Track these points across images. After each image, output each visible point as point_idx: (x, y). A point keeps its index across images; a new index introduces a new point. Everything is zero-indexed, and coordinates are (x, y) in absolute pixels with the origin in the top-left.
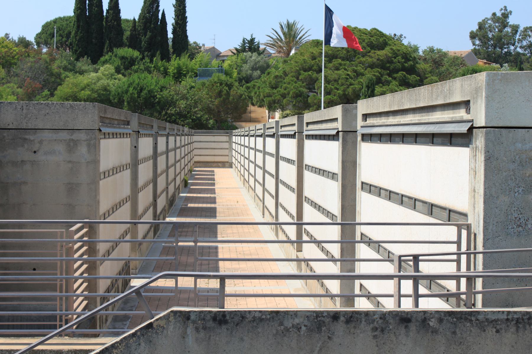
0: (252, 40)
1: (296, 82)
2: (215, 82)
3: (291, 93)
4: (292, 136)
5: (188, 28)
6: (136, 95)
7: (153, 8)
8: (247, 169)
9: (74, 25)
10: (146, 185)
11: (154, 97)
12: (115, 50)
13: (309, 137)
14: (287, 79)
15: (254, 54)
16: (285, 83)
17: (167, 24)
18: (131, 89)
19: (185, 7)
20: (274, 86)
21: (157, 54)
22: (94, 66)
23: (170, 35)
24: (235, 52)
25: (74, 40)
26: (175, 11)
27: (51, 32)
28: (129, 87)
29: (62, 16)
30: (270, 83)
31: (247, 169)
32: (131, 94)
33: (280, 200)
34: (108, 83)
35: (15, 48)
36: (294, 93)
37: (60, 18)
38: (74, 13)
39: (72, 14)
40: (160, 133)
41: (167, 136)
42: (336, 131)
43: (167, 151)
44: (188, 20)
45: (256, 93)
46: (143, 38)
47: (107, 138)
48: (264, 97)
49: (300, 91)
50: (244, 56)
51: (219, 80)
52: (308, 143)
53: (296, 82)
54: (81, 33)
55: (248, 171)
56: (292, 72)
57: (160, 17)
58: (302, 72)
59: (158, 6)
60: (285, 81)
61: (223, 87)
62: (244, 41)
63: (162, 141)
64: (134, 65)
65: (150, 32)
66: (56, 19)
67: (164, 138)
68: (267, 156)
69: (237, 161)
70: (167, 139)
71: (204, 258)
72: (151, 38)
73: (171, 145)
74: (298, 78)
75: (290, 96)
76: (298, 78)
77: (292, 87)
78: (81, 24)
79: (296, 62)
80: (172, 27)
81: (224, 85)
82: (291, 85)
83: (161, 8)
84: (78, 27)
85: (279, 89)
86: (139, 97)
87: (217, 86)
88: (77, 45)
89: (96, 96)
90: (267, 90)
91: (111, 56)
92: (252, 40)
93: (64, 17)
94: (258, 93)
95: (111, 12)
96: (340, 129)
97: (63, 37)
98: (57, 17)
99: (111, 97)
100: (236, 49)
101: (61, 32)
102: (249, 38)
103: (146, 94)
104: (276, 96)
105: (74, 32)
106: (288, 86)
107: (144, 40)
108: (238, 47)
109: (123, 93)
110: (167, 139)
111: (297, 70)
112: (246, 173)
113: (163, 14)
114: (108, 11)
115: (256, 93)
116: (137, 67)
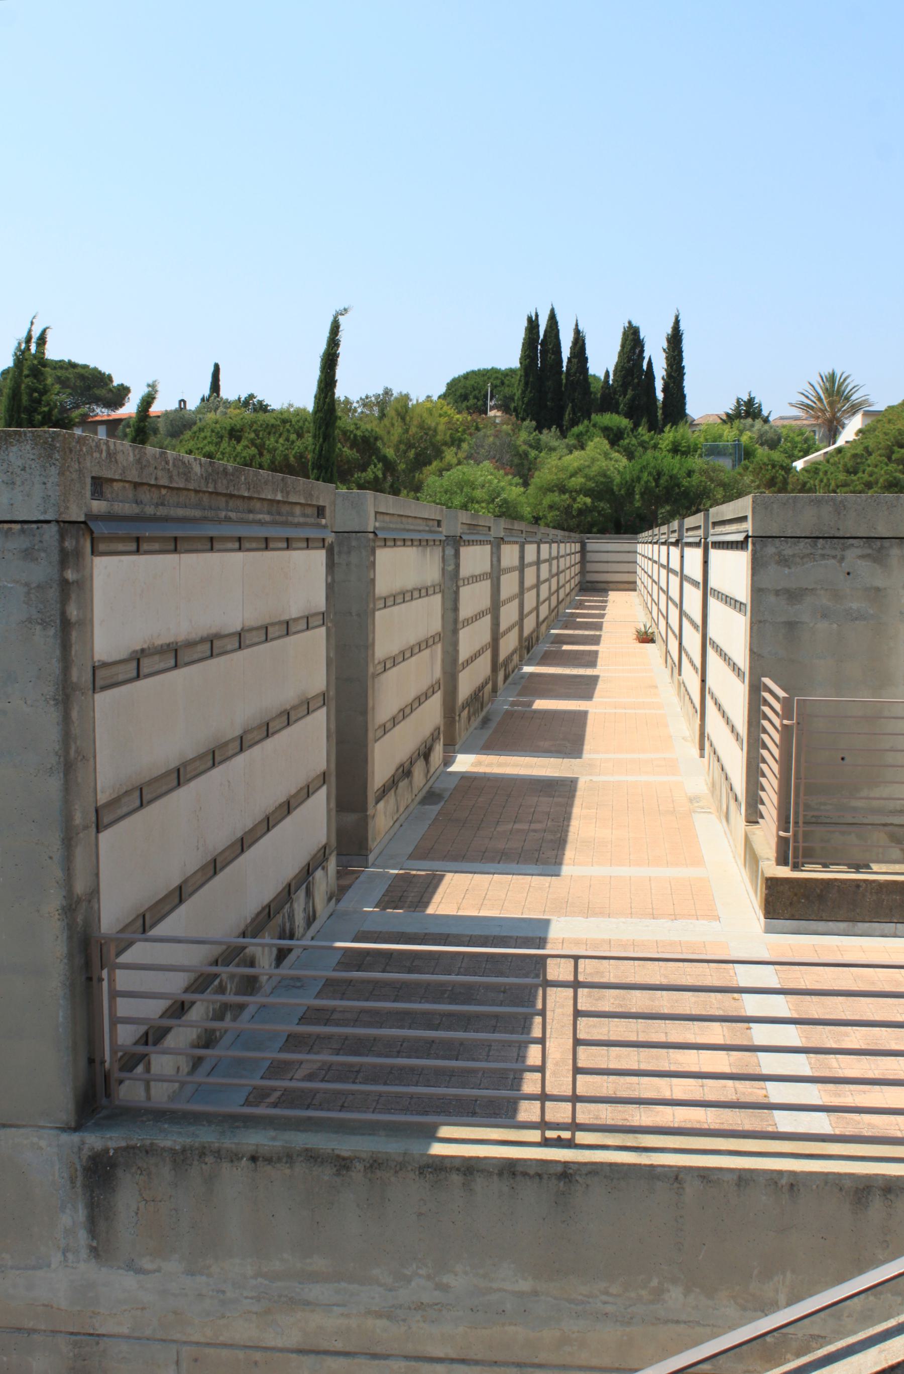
0: (750, 402)
1: (887, 465)
2: (764, 464)
3: (881, 480)
4: (697, 545)
5: (685, 383)
6: (654, 484)
7: (634, 353)
8: (665, 588)
9: (520, 381)
10: (530, 612)
11: (678, 485)
12: (593, 416)
13: (719, 545)
14: (872, 460)
15: (757, 421)
16: (869, 466)
17: (654, 378)
18: (645, 476)
19: (680, 352)
20: (851, 470)
21: (643, 423)
22: (567, 440)
23: (660, 395)
24: (724, 417)
25: (520, 403)
26: (667, 358)
27: (469, 392)
28: (641, 471)
29: (476, 369)
30: (845, 465)
31: (665, 588)
32: (646, 483)
33: (712, 633)
34: (607, 466)
35: (458, 416)
36: (886, 480)
37: (473, 372)
38: (521, 363)
39: (518, 365)
40: (528, 539)
41: (497, 544)
42: (744, 535)
43: (538, 563)
44: (685, 371)
45: (821, 481)
46: (621, 399)
47: (408, 546)
48: (837, 487)
49: (895, 478)
50: (741, 425)
51: (769, 460)
52: (714, 553)
53: (887, 465)
54: (531, 392)
55: (667, 593)
56: (879, 449)
57: (645, 367)
58: (896, 448)
59: (642, 351)
60: (869, 462)
61: (777, 471)
62: (738, 402)
63: (530, 549)
64: (623, 438)
65: (632, 390)
66: (468, 374)
67: (535, 546)
68: (670, 574)
69: (650, 581)
70: (539, 548)
71: (633, 711)
72: (633, 399)
73: (544, 555)
74: (889, 458)
75: (879, 485)
76: (889, 458)
77: (883, 472)
78: (531, 379)
79: (886, 434)
80: (662, 382)
81: (777, 468)
82: (879, 468)
83: (646, 355)
84: (526, 384)
85: (860, 475)
86: (657, 486)
87: (767, 470)
88: (525, 410)
89: (593, 485)
90: (842, 477)
91: (588, 426)
92: (750, 402)
93: (479, 370)
94: (825, 481)
95: (575, 361)
96: (750, 534)
97: (478, 400)
98: (469, 369)
99: (615, 488)
100: (728, 415)
101: (476, 392)
102: (746, 398)
103: (667, 481)
104: (856, 485)
105: (520, 391)
106: (876, 470)
107: (623, 402)
108: (730, 412)
109: (633, 481)
110: (539, 548)
111: (888, 446)
112: (663, 597)
113: (650, 363)
114: (569, 359)
115: (821, 481)
116: (627, 441)
